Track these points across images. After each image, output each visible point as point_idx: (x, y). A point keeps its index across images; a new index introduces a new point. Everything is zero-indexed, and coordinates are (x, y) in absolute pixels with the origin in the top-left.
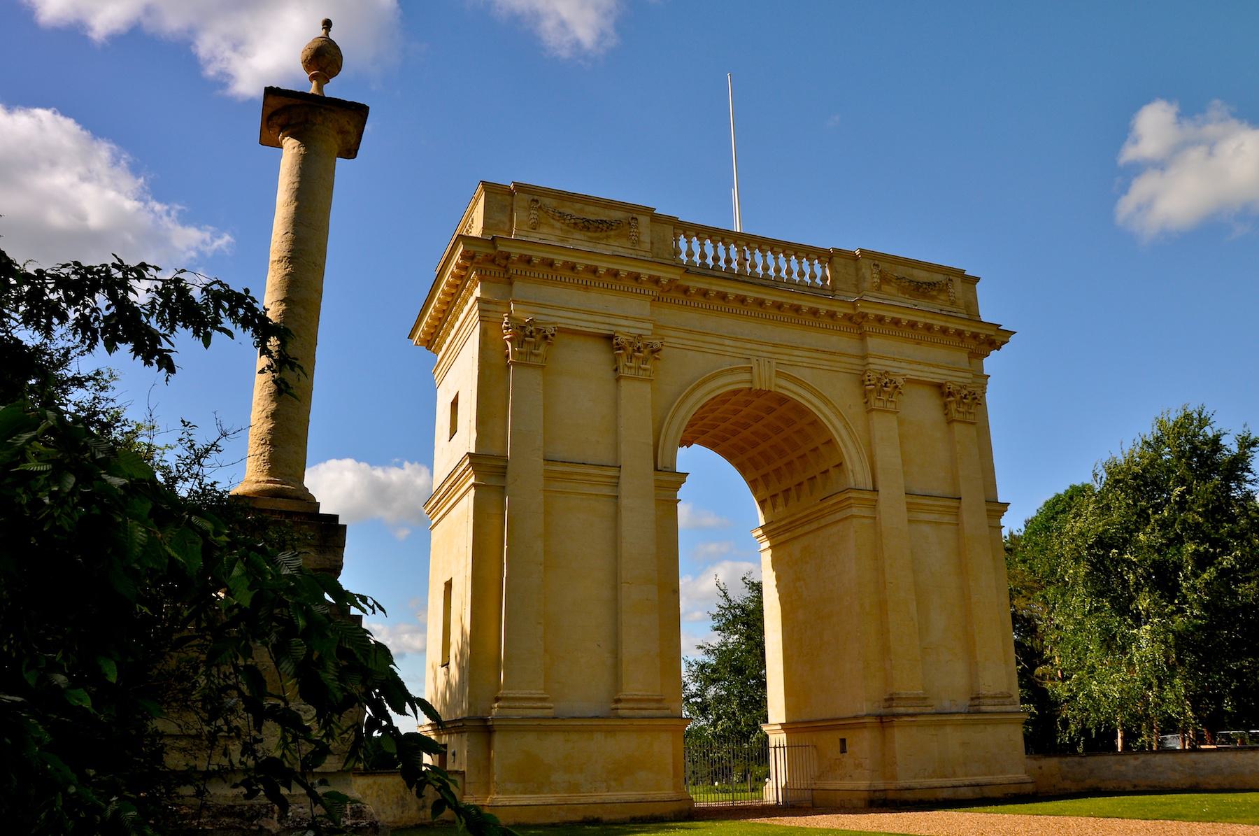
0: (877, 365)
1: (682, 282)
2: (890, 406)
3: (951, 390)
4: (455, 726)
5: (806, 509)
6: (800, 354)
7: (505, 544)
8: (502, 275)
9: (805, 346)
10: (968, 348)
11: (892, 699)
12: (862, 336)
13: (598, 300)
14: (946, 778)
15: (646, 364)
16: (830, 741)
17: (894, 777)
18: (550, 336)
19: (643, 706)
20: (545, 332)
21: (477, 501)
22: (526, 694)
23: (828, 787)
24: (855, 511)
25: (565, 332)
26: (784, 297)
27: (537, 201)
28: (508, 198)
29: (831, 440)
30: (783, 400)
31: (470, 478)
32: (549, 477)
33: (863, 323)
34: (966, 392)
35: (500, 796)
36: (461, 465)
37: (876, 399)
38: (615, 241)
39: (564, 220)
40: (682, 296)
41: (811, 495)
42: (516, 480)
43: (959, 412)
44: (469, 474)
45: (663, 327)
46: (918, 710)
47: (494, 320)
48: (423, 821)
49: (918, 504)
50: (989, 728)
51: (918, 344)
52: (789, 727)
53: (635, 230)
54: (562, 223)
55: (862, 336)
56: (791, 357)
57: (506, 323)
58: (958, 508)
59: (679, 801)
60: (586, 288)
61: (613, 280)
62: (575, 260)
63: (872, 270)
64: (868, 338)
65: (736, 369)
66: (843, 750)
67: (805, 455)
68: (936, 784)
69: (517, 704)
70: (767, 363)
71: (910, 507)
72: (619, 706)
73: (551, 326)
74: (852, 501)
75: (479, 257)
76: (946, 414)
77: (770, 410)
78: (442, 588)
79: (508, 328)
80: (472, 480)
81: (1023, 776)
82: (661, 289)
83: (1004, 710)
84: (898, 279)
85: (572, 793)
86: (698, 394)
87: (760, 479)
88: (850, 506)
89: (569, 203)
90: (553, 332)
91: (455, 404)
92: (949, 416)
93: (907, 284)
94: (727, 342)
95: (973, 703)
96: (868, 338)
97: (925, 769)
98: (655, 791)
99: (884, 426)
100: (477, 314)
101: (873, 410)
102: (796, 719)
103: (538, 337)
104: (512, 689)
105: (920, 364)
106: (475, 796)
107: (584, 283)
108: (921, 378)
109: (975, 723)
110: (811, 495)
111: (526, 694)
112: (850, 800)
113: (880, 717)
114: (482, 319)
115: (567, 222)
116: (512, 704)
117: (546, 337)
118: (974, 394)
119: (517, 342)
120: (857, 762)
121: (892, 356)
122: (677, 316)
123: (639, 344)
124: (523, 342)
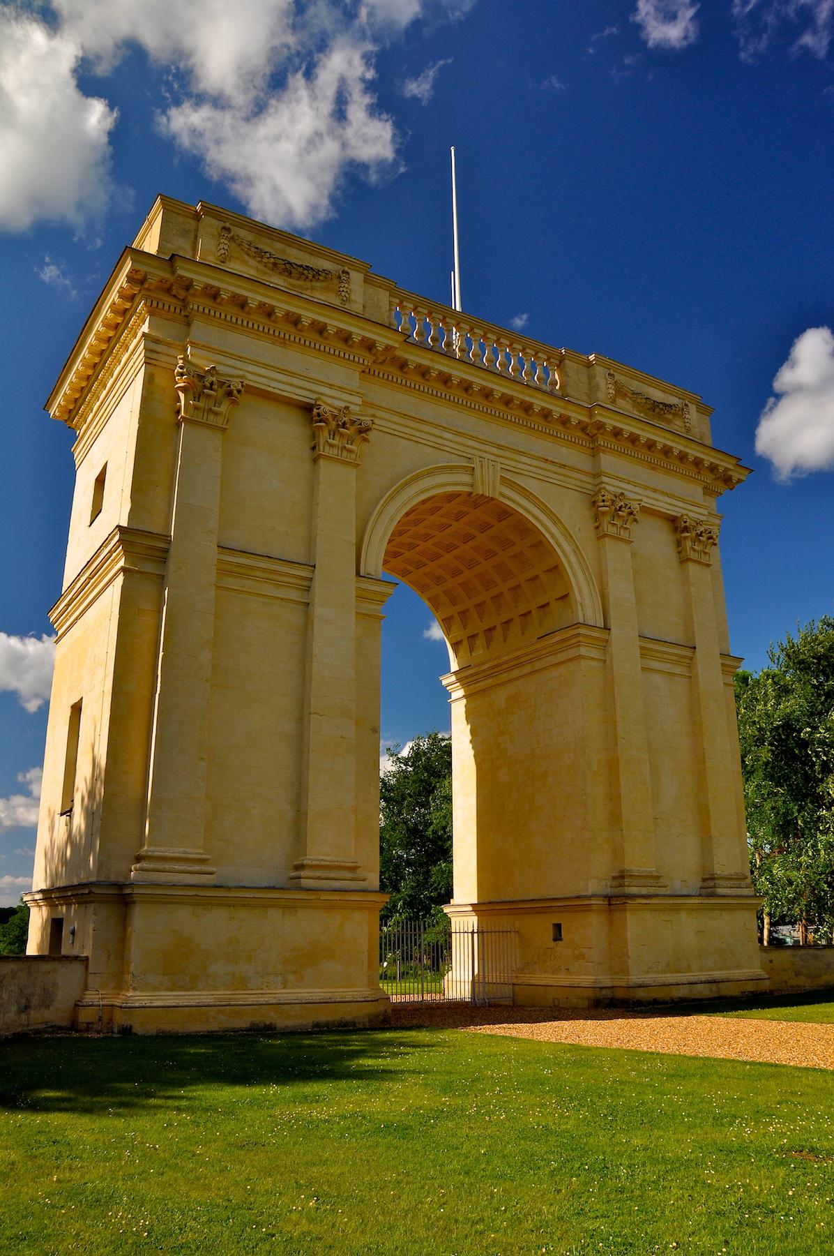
0: (612, 486)
1: (398, 353)
2: (624, 534)
3: (687, 524)
4: (77, 894)
5: (517, 650)
6: (526, 462)
7: (161, 650)
8: (178, 311)
9: (533, 453)
10: (704, 481)
11: (623, 877)
12: (595, 452)
13: (294, 359)
14: (680, 973)
15: (351, 444)
16: (540, 928)
17: (625, 971)
18: (235, 392)
19: (332, 875)
20: (229, 386)
21: (124, 588)
22: (179, 853)
23: (535, 982)
24: (583, 651)
25: (254, 394)
26: (515, 390)
27: (228, 230)
28: (193, 222)
29: (557, 566)
30: (504, 513)
31: (117, 562)
32: (224, 570)
33: (599, 435)
34: (702, 529)
35: (138, 993)
36: (106, 547)
37: (610, 523)
38: (321, 294)
39: (262, 257)
40: (397, 372)
41: (523, 634)
42: (181, 568)
43: (694, 550)
44: (115, 558)
45: (372, 405)
46: (651, 891)
47: (164, 365)
48: (25, 1028)
49: (650, 649)
50: (725, 915)
51: (653, 469)
52: (484, 908)
53: (346, 285)
54: (259, 262)
55: (595, 452)
56: (517, 464)
57: (181, 368)
58: (691, 658)
59: (375, 1001)
60: (284, 342)
61: (317, 337)
62: (273, 303)
63: (607, 380)
64: (601, 454)
65: (456, 467)
66: (558, 937)
67: (519, 586)
68: (671, 981)
69: (167, 867)
70: (490, 465)
71: (645, 653)
72: (303, 874)
73: (238, 380)
74: (581, 639)
75: (152, 281)
76: (679, 553)
77: (485, 527)
78: (68, 712)
79: (182, 375)
80: (122, 563)
81: (757, 971)
82: (374, 358)
83: (740, 894)
84: (633, 394)
85: (237, 990)
86: (412, 490)
87: (456, 616)
88: (578, 645)
89: (268, 241)
90: (240, 387)
91: (100, 481)
92: (683, 554)
93: (644, 401)
94: (446, 435)
95: (706, 884)
96: (601, 454)
97: (659, 962)
98: (344, 987)
99: (616, 554)
100: (143, 354)
101: (605, 536)
102: (482, 902)
103: (221, 392)
104: (160, 846)
105: (655, 491)
106: (101, 992)
107: (282, 335)
108: (655, 508)
109: (713, 908)
110: (523, 634)
111: (179, 853)
112: (567, 998)
113: (609, 898)
114: (149, 355)
115: (265, 260)
116: (160, 866)
117: (230, 394)
118: (710, 533)
119: (192, 395)
120: (576, 952)
121: (627, 478)
122: (386, 395)
123: (346, 419)
124: (200, 395)
